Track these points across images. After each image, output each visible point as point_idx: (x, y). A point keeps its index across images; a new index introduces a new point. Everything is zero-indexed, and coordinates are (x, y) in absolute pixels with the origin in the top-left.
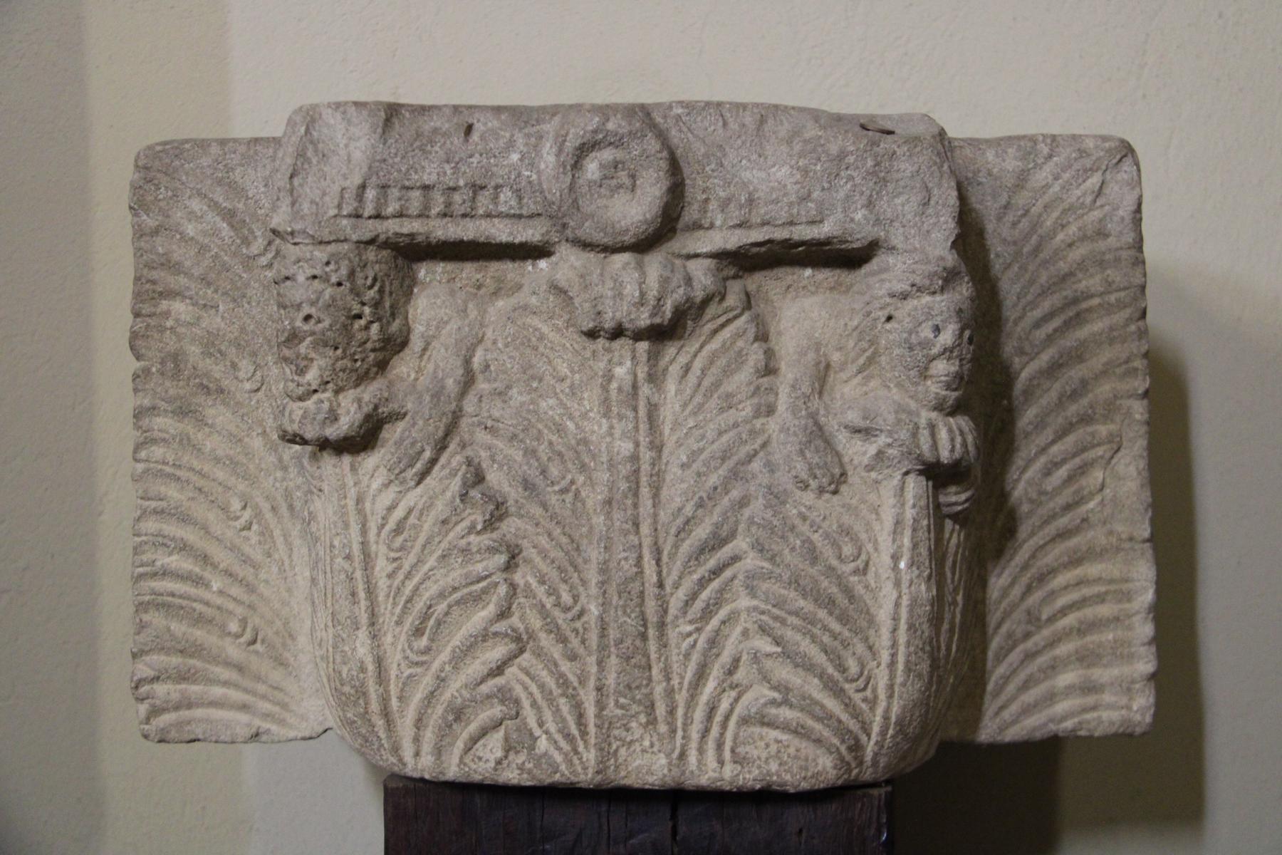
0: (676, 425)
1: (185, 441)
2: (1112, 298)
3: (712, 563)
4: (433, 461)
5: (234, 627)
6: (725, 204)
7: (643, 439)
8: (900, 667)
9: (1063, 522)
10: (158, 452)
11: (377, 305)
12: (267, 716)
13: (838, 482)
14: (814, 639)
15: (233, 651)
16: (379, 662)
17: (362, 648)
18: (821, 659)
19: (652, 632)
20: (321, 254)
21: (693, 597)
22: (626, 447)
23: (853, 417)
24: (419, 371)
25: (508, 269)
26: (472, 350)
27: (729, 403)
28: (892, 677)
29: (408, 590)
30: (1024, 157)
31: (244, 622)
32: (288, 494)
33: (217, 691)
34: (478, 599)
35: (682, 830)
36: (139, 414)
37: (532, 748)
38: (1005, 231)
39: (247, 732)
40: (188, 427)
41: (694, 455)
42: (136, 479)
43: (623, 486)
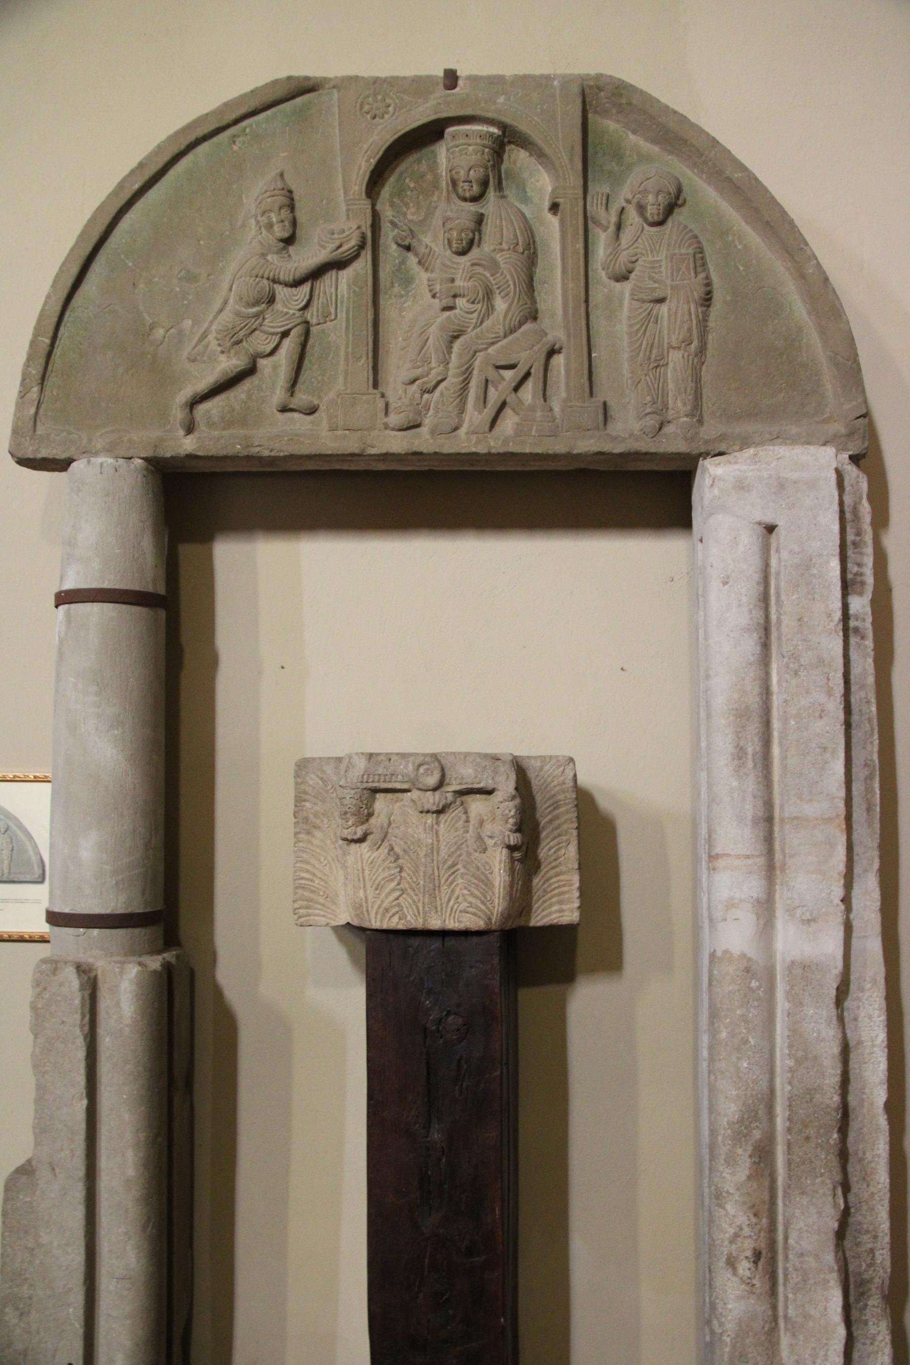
0: (443, 836)
1: (309, 842)
2: (567, 801)
3: (452, 871)
4: (381, 845)
5: (321, 893)
6: (456, 779)
7: (435, 839)
8: (501, 898)
9: (553, 864)
10: (301, 844)
11: (366, 805)
12: (331, 919)
13: (485, 850)
14: (478, 890)
15: (321, 900)
16: (366, 897)
17: (361, 894)
18: (480, 895)
19: (437, 889)
20: (353, 792)
21: (447, 880)
22: (430, 841)
23: (489, 833)
24: (377, 821)
25: (399, 795)
26: (391, 816)
27: (457, 830)
28: (499, 901)
29: (374, 878)
30: (542, 762)
31: (324, 892)
32: (337, 856)
33: (317, 912)
34: (392, 880)
35: (446, 944)
36: (296, 834)
37: (406, 918)
38: (537, 783)
39: (325, 923)
40: (309, 837)
41: (448, 843)
42: (295, 852)
43: (430, 851)
